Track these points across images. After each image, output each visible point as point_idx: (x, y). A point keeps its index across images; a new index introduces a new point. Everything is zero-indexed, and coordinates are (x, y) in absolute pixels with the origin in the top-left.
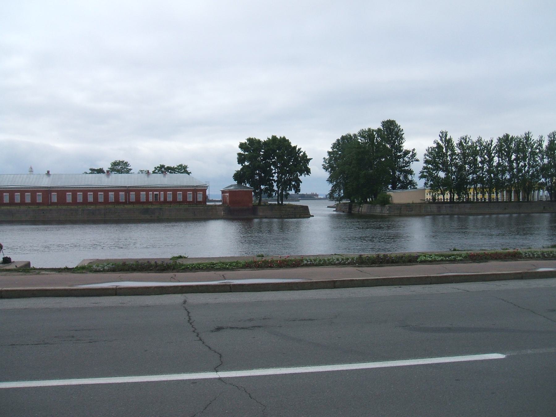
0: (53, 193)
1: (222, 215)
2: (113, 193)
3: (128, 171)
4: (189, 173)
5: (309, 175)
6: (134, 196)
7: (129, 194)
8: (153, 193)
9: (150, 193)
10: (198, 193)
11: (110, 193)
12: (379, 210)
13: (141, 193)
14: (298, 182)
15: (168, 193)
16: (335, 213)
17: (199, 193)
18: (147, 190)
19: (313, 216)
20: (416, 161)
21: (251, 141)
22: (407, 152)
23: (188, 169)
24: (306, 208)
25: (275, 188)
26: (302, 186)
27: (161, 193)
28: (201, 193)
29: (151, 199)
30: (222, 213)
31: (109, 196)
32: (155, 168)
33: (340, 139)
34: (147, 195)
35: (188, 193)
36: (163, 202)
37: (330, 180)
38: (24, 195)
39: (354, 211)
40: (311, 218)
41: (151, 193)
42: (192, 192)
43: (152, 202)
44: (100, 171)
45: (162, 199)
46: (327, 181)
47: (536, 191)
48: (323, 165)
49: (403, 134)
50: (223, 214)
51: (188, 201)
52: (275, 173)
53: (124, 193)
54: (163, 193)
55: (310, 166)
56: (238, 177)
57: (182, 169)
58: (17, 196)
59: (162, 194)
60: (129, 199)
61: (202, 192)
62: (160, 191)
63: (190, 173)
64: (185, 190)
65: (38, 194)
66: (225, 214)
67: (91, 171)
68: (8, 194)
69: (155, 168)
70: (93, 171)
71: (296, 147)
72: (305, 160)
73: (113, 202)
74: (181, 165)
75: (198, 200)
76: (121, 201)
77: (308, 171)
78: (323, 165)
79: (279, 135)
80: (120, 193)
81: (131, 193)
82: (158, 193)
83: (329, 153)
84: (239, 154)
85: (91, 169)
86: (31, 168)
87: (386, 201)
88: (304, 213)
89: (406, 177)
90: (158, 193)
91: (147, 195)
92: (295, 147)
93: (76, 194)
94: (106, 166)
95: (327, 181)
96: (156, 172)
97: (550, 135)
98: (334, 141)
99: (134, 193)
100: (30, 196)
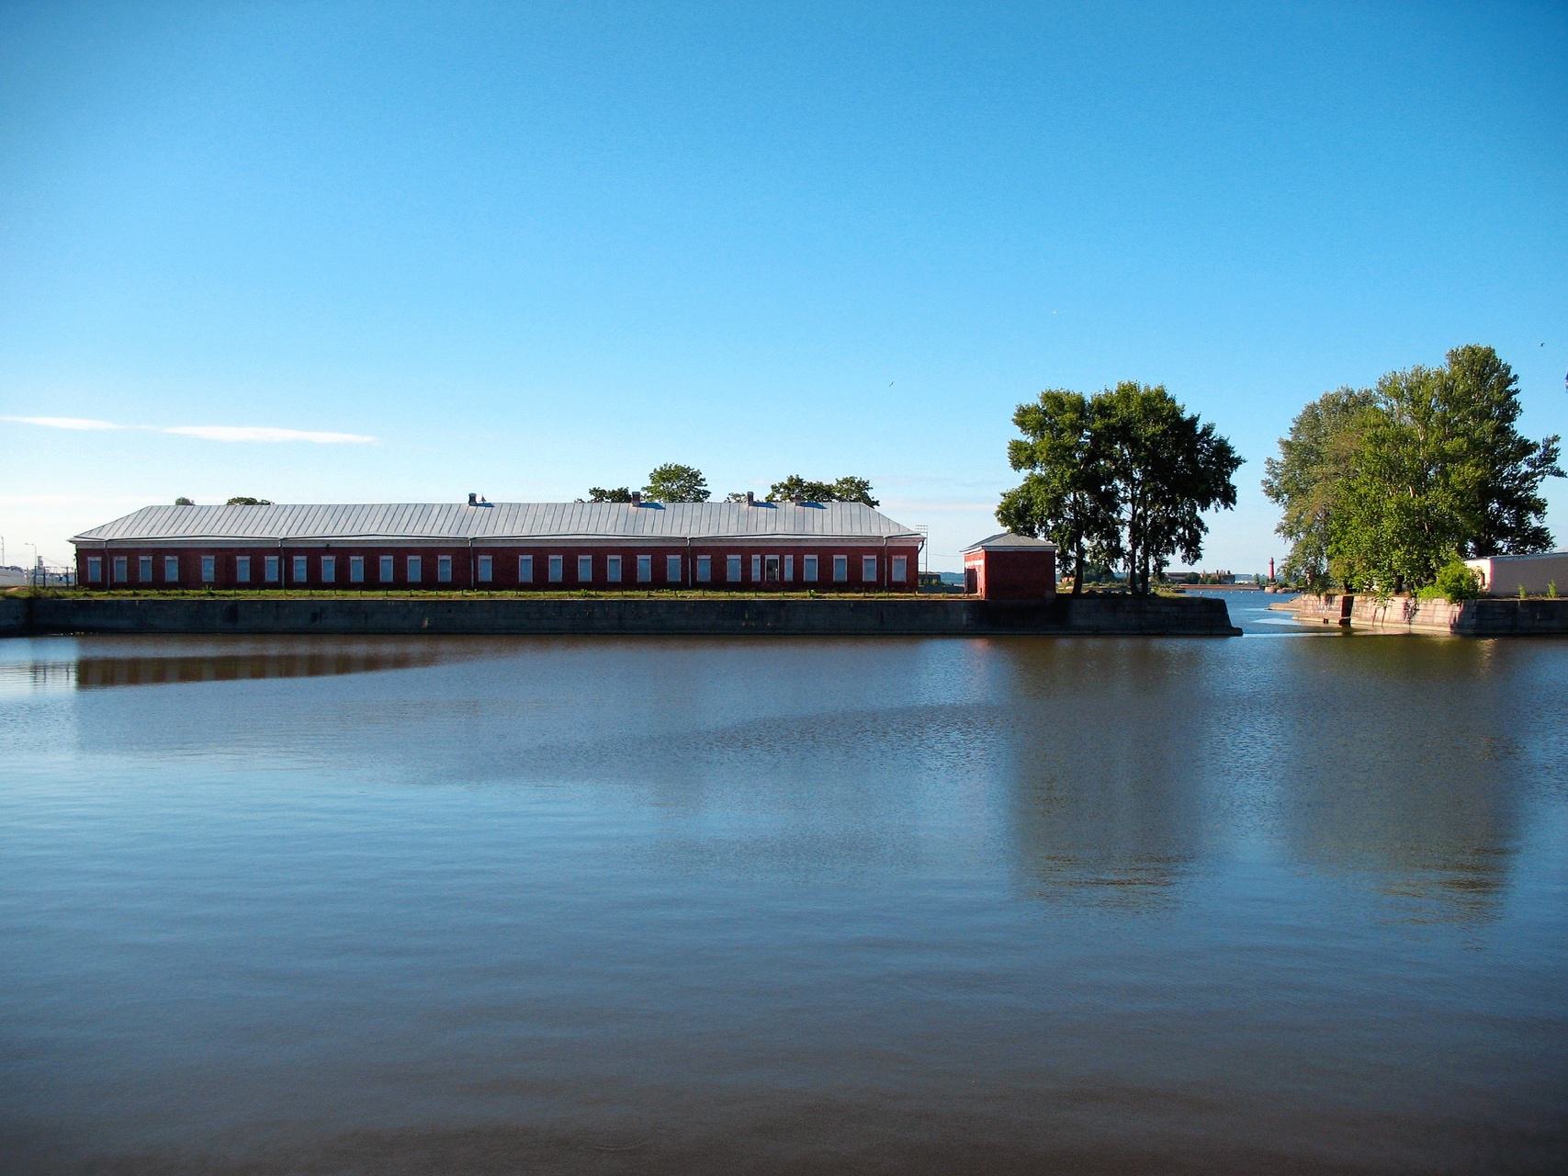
1: (964, 623)
2: (649, 557)
3: (701, 496)
4: (872, 504)
5: (1231, 509)
8: (763, 559)
10: (894, 557)
11: (639, 557)
12: (1442, 614)
13: (729, 557)
14: (1195, 529)
15: (806, 557)
17: (897, 557)
18: (747, 550)
20: (1554, 474)
21: (1056, 401)
22: (1525, 448)
23: (870, 494)
24: (1218, 607)
25: (1125, 542)
26: (1206, 541)
27: (787, 557)
28: (902, 557)
29: (756, 575)
30: (964, 617)
31: (636, 566)
32: (773, 487)
34: (746, 565)
35: (865, 557)
36: (790, 582)
37: (1288, 530)
38: (634, 564)
39: (1360, 618)
40: (1233, 640)
41: (758, 557)
42: (875, 557)
43: (760, 583)
44: (621, 496)
45: (789, 575)
46: (1278, 531)
47: (1468, 567)
48: (1264, 482)
49: (1516, 392)
50: (968, 619)
51: (865, 583)
52: (1125, 500)
53: (679, 557)
55: (1235, 478)
56: (1016, 513)
57: (857, 492)
58: (385, 564)
59: (789, 560)
60: (694, 576)
61: (905, 557)
62: (782, 550)
63: (877, 503)
64: (854, 552)
66: (972, 619)
67: (593, 497)
69: (773, 487)
70: (599, 495)
71: (1197, 419)
72: (1225, 458)
73: (619, 583)
74: (850, 481)
75: (894, 579)
76: (324, 579)
77: (1229, 497)
78: (1264, 482)
79: (1148, 382)
81: (699, 557)
82: (777, 557)
83: (1287, 445)
84: (1017, 448)
85: (593, 492)
89: (1520, 520)
90: (777, 557)
91: (746, 565)
92: (1194, 421)
94: (638, 482)
95: (1278, 531)
96: (774, 499)
98: (1298, 411)
99: (709, 557)
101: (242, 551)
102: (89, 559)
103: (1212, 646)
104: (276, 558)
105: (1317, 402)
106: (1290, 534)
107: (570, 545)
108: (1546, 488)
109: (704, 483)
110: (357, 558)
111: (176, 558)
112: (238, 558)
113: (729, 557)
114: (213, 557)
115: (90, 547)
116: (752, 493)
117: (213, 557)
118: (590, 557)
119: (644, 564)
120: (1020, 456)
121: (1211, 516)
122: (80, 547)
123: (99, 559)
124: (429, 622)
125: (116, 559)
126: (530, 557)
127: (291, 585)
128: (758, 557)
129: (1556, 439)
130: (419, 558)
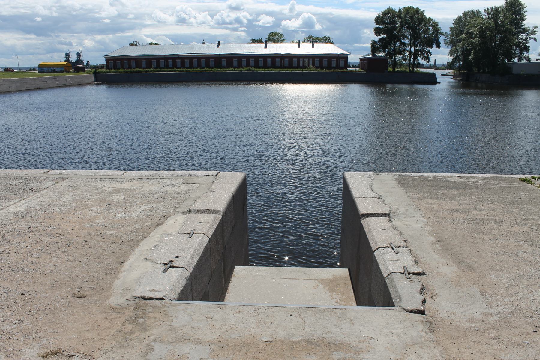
0: (222, 60)
2: (271, 59)
6: (171, 63)
7: (284, 60)
9: (301, 59)
11: (268, 59)
14: (429, 53)
16: (452, 80)
19: (440, 83)
21: (389, 12)
22: (525, 31)
23: (332, 40)
29: (301, 64)
33: (462, 15)
37: (451, 54)
38: (323, 61)
40: (438, 85)
41: (302, 59)
46: (448, 55)
53: (279, 59)
54: (311, 59)
59: (163, 61)
65: (211, 60)
68: (188, 60)
69: (305, 38)
80: (276, 59)
81: (285, 59)
83: (451, 28)
86: (203, 41)
87: (347, 70)
88: (432, 80)
91: (303, 61)
93: (193, 61)
97: (523, 25)
100: (188, 62)
101: (154, 59)
102: (109, 62)
103: (431, 87)
104: (163, 60)
105: (374, 32)
106: (451, 55)
107: (186, 57)
108: (531, 44)
109: (284, 37)
110: (187, 60)
111: (135, 61)
112: (152, 61)
113: (294, 59)
114: (145, 61)
115: (109, 58)
116: (265, 48)
117: (145, 61)
118: (254, 59)
119: (269, 61)
120: (378, 31)
121: (434, 49)
122: (107, 58)
123: (112, 62)
124: (380, 52)
125: (117, 62)
126: (237, 59)
127: (168, 68)
128: (302, 59)
129: (536, 27)
130: (204, 60)
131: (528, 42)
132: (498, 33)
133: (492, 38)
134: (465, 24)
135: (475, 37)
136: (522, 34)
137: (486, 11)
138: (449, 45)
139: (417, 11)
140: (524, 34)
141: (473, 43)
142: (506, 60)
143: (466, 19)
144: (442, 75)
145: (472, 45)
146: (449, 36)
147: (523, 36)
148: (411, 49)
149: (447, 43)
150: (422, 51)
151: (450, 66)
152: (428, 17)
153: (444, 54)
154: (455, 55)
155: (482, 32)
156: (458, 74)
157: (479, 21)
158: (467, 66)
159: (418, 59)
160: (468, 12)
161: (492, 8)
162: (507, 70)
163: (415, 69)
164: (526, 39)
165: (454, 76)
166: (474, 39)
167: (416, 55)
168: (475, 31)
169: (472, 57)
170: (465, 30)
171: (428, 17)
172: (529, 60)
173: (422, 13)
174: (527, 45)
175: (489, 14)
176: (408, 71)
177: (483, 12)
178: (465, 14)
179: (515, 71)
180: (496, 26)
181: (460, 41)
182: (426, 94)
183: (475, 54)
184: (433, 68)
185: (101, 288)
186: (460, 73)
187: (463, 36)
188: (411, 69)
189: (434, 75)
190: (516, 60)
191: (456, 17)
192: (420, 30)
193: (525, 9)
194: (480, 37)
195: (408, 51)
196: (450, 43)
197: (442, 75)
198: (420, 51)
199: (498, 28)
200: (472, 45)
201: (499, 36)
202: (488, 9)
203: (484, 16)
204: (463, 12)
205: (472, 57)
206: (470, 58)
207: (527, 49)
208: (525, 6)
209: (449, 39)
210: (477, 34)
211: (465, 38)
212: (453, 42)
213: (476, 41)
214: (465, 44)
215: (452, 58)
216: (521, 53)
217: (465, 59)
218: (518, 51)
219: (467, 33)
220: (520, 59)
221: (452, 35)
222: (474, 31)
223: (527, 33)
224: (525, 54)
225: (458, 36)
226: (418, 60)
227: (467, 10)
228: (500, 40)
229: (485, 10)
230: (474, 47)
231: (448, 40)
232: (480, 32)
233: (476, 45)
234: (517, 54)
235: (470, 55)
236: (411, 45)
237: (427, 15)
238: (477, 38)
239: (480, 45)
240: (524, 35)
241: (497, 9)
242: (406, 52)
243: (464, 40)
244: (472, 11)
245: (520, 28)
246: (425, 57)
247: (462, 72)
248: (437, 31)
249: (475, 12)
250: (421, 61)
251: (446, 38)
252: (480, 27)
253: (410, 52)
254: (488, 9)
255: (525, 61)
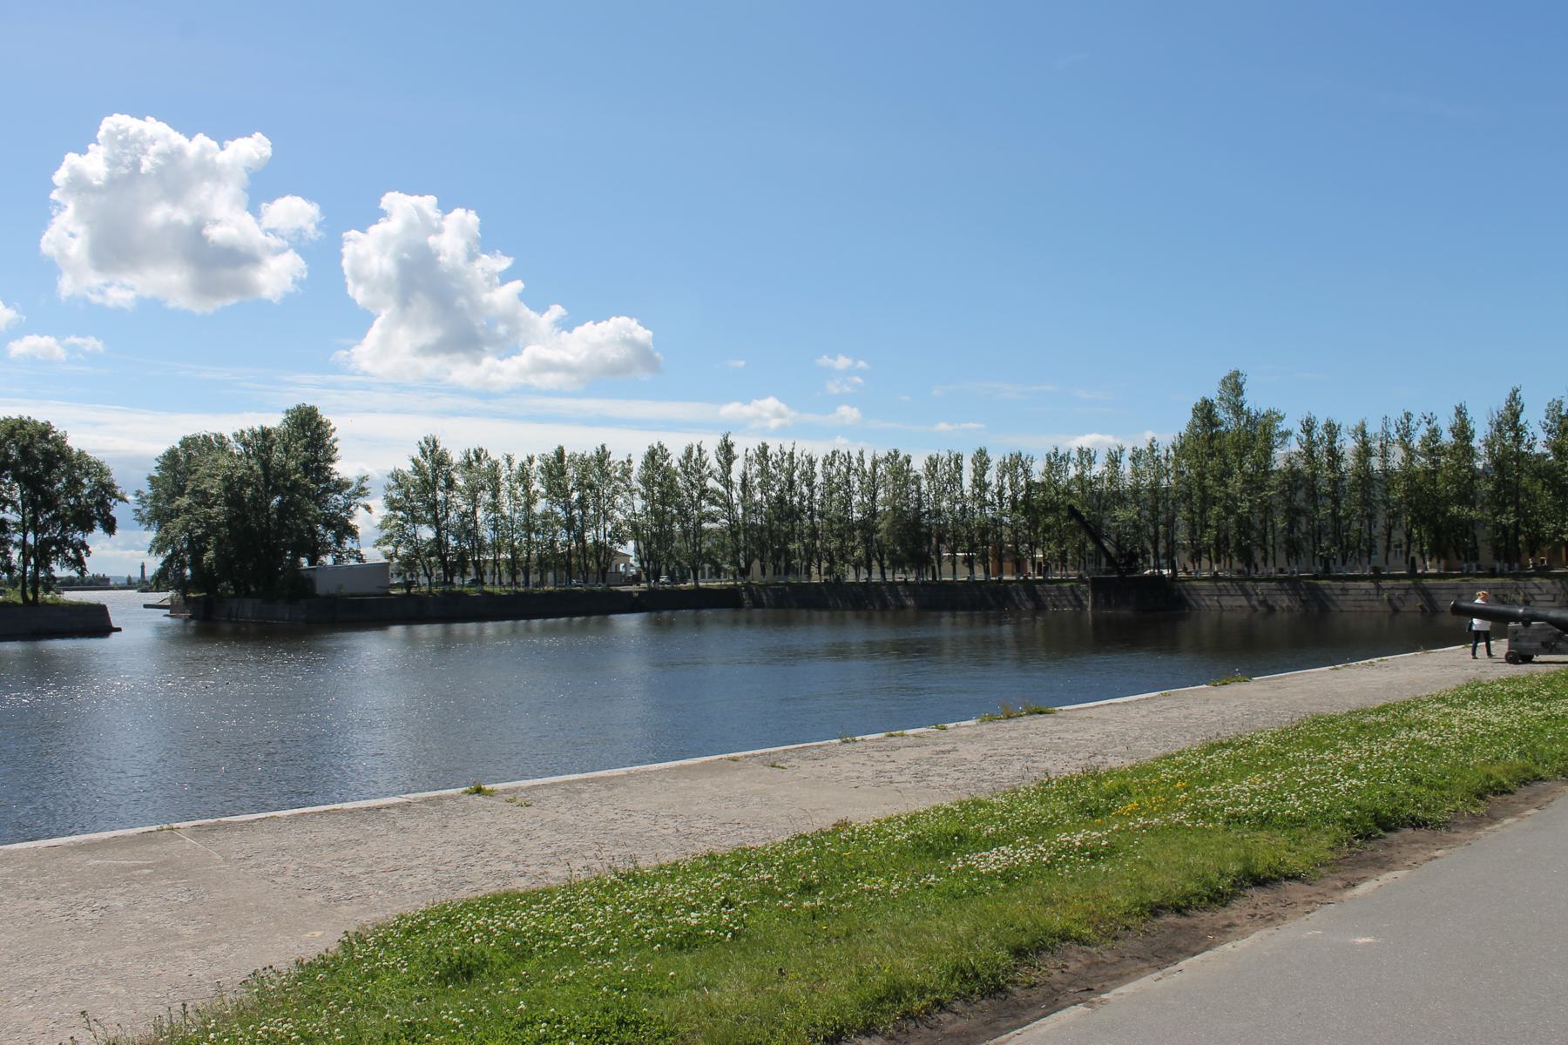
19: (119, 630)
22: (341, 486)
33: (178, 446)
37: (158, 547)
40: (114, 635)
59: (1007, 574)
88: (96, 623)
131: (351, 515)
132: (276, 491)
133: (259, 506)
134: (188, 469)
135: (215, 503)
136: (335, 496)
137: (239, 437)
138: (149, 525)
139: (44, 431)
140: (340, 494)
141: (211, 517)
142: (304, 562)
143: (189, 457)
144: (146, 606)
145: (208, 524)
146: (149, 501)
147: (340, 499)
148: (25, 537)
149: (143, 520)
150: (62, 544)
151: (159, 581)
152: (76, 450)
153: (138, 549)
154: (170, 551)
155: (233, 489)
156: (183, 601)
157: (224, 461)
158: (204, 578)
159: (51, 565)
160: (194, 439)
161: (252, 430)
162: (301, 587)
163: (41, 594)
164: (347, 507)
165: (173, 608)
166: (211, 507)
167: (41, 555)
168: (214, 487)
169: (210, 554)
170: (190, 486)
171: (76, 450)
172: (360, 559)
173: (59, 442)
174: (351, 522)
175: (245, 444)
176: (21, 602)
177: (232, 439)
178: (187, 443)
179: (322, 587)
180: (266, 474)
181: (176, 513)
182: (76, 671)
183: (217, 549)
184: (135, 588)
185: (1306, 836)
186: (188, 601)
187: (184, 501)
188: (31, 597)
189: (101, 610)
190: (328, 560)
191: (162, 449)
192: (51, 484)
193: (334, 436)
194: (228, 502)
195: (16, 545)
196: (151, 519)
197: (146, 606)
198: (54, 541)
199: (273, 478)
200: (208, 524)
201: (275, 501)
202: (243, 432)
203: (237, 449)
204: (180, 438)
205: (210, 554)
206: (205, 558)
207: (352, 532)
208: (332, 427)
209: (148, 509)
210: (219, 496)
211: (190, 504)
212: (159, 515)
213: (218, 514)
214: (191, 520)
215: (161, 559)
216: (339, 543)
217: (196, 563)
218: (330, 536)
219: (194, 492)
220: (338, 559)
221: (156, 497)
222: (212, 487)
223: (348, 492)
224: (348, 544)
225: (171, 498)
226: (51, 569)
227: (189, 434)
228: (278, 510)
229: (235, 435)
230: (212, 529)
231: (144, 512)
232: (227, 489)
233: (220, 525)
234: (330, 544)
235: (206, 550)
236: (24, 525)
237: (75, 442)
238: (220, 505)
239: (229, 524)
240: (339, 497)
241: (265, 434)
242: (11, 549)
243: (187, 511)
244: (205, 436)
245: (327, 479)
246: (70, 559)
247: (193, 595)
248: (106, 491)
249: (213, 438)
250: (60, 571)
251: (140, 507)
252: (225, 478)
253: (23, 545)
254: (243, 432)
255: (353, 562)
